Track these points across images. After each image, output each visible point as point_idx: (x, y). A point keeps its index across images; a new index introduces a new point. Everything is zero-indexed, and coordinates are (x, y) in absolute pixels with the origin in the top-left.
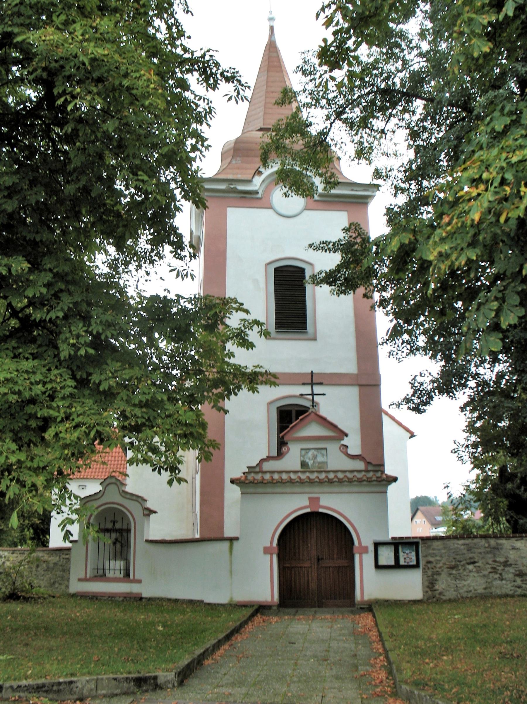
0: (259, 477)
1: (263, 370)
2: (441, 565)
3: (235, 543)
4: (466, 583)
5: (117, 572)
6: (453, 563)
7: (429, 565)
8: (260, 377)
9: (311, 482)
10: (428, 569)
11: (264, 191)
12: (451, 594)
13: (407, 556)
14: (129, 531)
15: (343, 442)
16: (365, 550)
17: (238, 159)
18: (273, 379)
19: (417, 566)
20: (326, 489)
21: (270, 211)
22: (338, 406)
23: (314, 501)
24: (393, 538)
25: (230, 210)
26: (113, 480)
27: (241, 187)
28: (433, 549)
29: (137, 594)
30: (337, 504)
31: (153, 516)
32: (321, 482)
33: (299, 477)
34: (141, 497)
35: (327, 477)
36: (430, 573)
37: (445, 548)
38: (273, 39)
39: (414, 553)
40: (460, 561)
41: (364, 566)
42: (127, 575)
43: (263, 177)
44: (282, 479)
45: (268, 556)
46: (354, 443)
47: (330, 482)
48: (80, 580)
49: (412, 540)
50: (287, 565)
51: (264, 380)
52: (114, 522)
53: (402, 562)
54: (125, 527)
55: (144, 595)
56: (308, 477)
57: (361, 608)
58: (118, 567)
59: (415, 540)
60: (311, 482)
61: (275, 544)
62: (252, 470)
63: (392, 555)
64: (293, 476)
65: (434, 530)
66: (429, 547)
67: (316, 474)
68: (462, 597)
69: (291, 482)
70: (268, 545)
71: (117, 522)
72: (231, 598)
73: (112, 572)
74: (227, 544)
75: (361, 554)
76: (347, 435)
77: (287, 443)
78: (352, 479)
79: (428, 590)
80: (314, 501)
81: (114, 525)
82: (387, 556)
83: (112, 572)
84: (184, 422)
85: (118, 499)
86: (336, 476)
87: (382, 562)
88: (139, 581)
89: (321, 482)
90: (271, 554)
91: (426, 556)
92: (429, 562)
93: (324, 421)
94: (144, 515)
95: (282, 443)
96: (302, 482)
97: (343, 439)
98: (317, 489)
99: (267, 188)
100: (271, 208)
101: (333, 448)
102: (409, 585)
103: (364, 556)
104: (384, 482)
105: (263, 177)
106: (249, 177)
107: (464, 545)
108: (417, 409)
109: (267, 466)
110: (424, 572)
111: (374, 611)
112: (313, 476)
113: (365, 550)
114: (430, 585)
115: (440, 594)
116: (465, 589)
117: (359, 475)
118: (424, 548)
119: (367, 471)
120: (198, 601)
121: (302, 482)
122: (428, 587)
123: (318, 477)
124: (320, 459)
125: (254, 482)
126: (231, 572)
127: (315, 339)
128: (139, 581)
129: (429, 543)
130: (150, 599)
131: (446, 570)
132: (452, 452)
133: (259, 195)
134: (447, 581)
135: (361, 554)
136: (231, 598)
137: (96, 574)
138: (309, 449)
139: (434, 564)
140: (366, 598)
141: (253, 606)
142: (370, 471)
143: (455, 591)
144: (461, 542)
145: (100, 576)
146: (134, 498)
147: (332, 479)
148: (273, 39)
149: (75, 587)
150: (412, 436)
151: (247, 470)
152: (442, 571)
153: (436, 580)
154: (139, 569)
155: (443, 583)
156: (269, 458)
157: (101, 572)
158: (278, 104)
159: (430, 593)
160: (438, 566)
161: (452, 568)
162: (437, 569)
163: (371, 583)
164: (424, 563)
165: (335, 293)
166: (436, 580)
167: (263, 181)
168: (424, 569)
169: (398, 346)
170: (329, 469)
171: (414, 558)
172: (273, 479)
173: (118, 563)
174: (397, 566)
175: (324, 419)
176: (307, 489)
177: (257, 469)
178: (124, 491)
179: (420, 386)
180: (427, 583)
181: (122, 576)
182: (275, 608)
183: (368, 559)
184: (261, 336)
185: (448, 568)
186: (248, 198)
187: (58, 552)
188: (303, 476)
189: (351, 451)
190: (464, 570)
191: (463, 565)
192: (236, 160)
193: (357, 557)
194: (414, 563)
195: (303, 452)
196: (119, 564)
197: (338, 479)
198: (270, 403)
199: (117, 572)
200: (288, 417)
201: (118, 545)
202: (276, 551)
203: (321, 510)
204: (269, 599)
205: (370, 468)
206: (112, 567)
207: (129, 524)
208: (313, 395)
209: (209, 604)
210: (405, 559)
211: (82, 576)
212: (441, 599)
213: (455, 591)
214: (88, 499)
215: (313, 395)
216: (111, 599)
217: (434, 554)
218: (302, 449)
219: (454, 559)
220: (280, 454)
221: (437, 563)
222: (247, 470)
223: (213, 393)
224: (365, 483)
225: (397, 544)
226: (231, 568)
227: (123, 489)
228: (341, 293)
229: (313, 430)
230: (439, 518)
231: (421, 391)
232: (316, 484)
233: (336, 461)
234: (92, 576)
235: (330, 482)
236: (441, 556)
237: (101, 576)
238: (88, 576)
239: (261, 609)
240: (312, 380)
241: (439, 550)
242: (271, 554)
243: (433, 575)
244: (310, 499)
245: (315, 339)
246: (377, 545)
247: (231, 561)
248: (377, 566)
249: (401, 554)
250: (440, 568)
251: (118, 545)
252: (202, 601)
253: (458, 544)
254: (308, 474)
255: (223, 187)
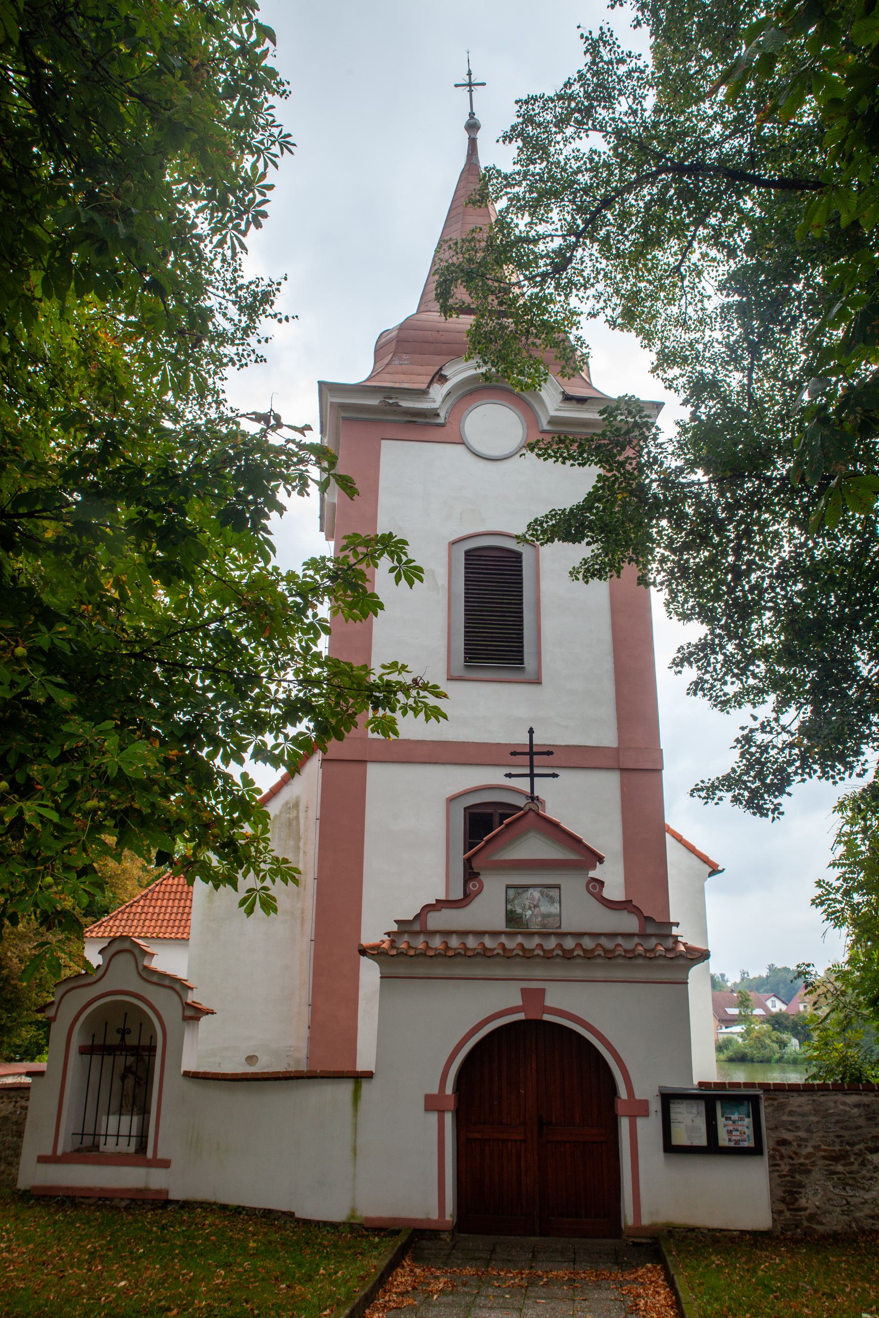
0: (419, 943)
1: (406, 679)
2: (810, 1149)
3: (365, 1086)
4: (868, 1196)
5: (123, 1141)
6: (837, 1148)
7: (783, 1149)
8: (400, 696)
9: (527, 955)
10: (782, 1157)
11: (450, 412)
12: (834, 1222)
13: (735, 1127)
14: (152, 1049)
15: (592, 874)
16: (641, 1109)
17: (404, 357)
18: (432, 701)
19: (756, 1151)
20: (559, 973)
21: (460, 449)
22: (582, 804)
23: (533, 997)
24: (701, 1084)
25: (384, 443)
26: (127, 945)
27: (405, 404)
28: (791, 1113)
29: (158, 1192)
30: (580, 1002)
31: (204, 1019)
32: (548, 956)
33: (503, 945)
34: (179, 980)
35: (560, 946)
36: (785, 1169)
37: (816, 1112)
38: (474, 161)
39: (748, 1121)
40: (852, 1145)
41: (640, 1142)
42: (142, 1148)
43: (448, 386)
44: (466, 949)
45: (434, 1117)
46: (613, 877)
47: (568, 956)
48: (42, 1159)
49: (743, 1092)
50: (477, 1136)
51: (411, 701)
52: (124, 1032)
53: (723, 1140)
54: (145, 1042)
55: (173, 1196)
56: (521, 945)
57: (635, 1244)
58: (124, 1131)
59: (751, 1092)
60: (527, 955)
61: (449, 1090)
62: (407, 928)
63: (701, 1123)
64: (489, 942)
65: (724, 1030)
66: (781, 1108)
67: (536, 940)
68: (863, 1231)
69: (485, 954)
70: (435, 1091)
71: (129, 1032)
72: (353, 1210)
73: (111, 1141)
74: (345, 1089)
75: (633, 1118)
76: (601, 859)
77: (479, 874)
78: (613, 951)
79: (782, 1207)
80: (533, 997)
81: (123, 1039)
82: (689, 1125)
83: (111, 1141)
84: (112, 772)
85: (135, 984)
86: (579, 945)
87: (680, 1138)
88: (165, 1164)
89: (548, 956)
90: (441, 1112)
91: (776, 1128)
92: (783, 1142)
93: (555, 831)
94: (185, 1019)
95: (471, 874)
96: (507, 955)
97: (594, 867)
98: (539, 973)
99: (454, 406)
100: (462, 442)
101: (572, 886)
102: (738, 1195)
103: (640, 1122)
104: (682, 962)
105: (448, 386)
106: (424, 386)
107: (857, 1106)
108: (755, 804)
109: (435, 921)
110: (774, 1166)
111: (669, 1259)
112: (532, 943)
113: (641, 1109)
114: (787, 1194)
115: (812, 1218)
116: (867, 1211)
117: (628, 945)
118: (770, 1109)
119: (643, 935)
120: (284, 1213)
121: (507, 955)
122: (783, 1200)
123: (540, 946)
124: (546, 908)
125: (413, 953)
126: (355, 1154)
127: (538, 682)
128: (165, 1164)
129: (781, 1098)
130: (186, 1205)
131: (821, 1162)
132: (813, 901)
133: (441, 420)
134: (825, 1188)
135: (633, 1118)
136: (353, 1210)
137: (78, 1146)
138: (527, 887)
139: (794, 1147)
140: (645, 1221)
141: (396, 1233)
142: (651, 935)
143: (843, 1213)
144: (853, 1099)
145: (88, 1150)
146: (167, 982)
147: (572, 950)
148: (474, 161)
149: (32, 1174)
150: (715, 870)
151: (395, 928)
152: (813, 1164)
153: (801, 1185)
154: (167, 1139)
155: (815, 1194)
156: (440, 905)
157: (88, 1141)
158: (474, 203)
159: (788, 1214)
160: (804, 1152)
161: (835, 1158)
162: (802, 1160)
163: (658, 1188)
164: (772, 1144)
165: (580, 576)
166: (801, 1185)
167: (449, 394)
168: (772, 1157)
169: (715, 670)
170: (564, 929)
171: (749, 1132)
172: (447, 948)
173: (125, 1119)
174: (712, 1148)
175: (556, 825)
176: (517, 972)
177: (417, 927)
178: (146, 968)
179: (762, 754)
180: (780, 1193)
181: (132, 1149)
182: (445, 1236)
183: (649, 1129)
184: (398, 580)
185: (824, 1158)
186: (420, 424)
187: (12, 1094)
188: (511, 944)
189: (607, 893)
190: (863, 1164)
191: (859, 1154)
192: (401, 359)
193: (624, 1124)
194: (750, 1143)
195: (511, 892)
196: (128, 1123)
197: (584, 950)
198: (451, 800)
199: (123, 1141)
200: (483, 825)
201: (130, 1081)
202: (451, 1104)
203: (547, 1017)
204: (435, 1216)
205: (649, 931)
206: (112, 1130)
207: (153, 1037)
208: (532, 776)
209: (307, 1222)
210: (730, 1132)
211: (48, 1152)
212: (815, 1231)
213: (843, 1213)
214: (72, 984)
215: (532, 776)
216: (104, 1201)
217: (792, 1123)
218: (508, 887)
219: (838, 1137)
220: (468, 897)
221: (799, 1146)
222: (395, 928)
223: (286, 736)
224: (640, 961)
225: (713, 1098)
226: (355, 1141)
227: (146, 963)
228: (593, 575)
229: (533, 847)
230: (733, 1011)
231: (763, 764)
232: (538, 960)
233: (578, 913)
234: (69, 1149)
235: (568, 956)
236: (809, 1130)
237: (89, 1149)
238: (59, 1152)
239: (412, 1242)
240: (533, 757)
241: (803, 1115)
242: (441, 1112)
243: (792, 1173)
244: (524, 991)
245: (538, 682)
246: (668, 1098)
247: (355, 1125)
248: (670, 1148)
249: (721, 1121)
250: (808, 1156)
251: (130, 1081)
252: (291, 1214)
253: (844, 1104)
254: (519, 939)
255: (374, 401)
